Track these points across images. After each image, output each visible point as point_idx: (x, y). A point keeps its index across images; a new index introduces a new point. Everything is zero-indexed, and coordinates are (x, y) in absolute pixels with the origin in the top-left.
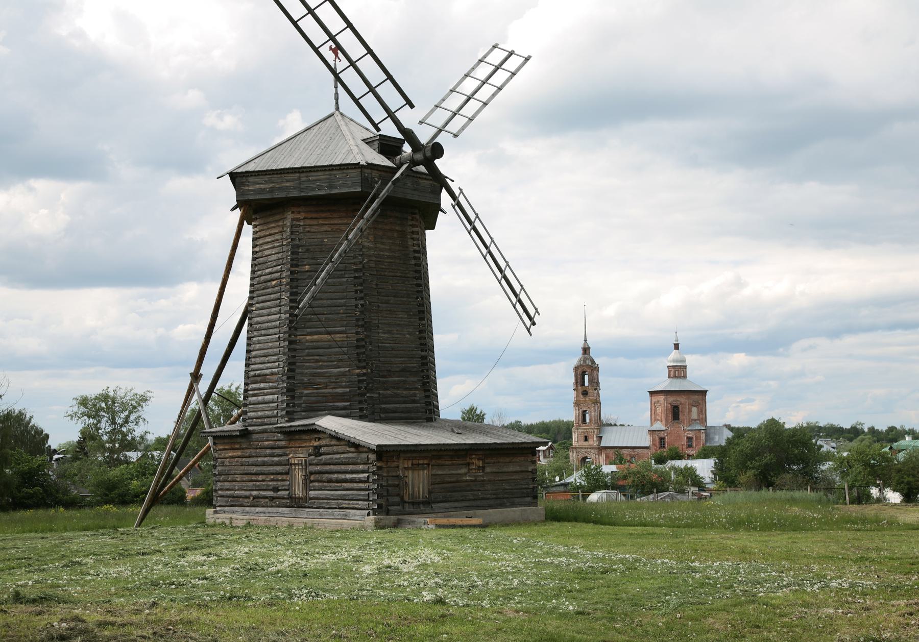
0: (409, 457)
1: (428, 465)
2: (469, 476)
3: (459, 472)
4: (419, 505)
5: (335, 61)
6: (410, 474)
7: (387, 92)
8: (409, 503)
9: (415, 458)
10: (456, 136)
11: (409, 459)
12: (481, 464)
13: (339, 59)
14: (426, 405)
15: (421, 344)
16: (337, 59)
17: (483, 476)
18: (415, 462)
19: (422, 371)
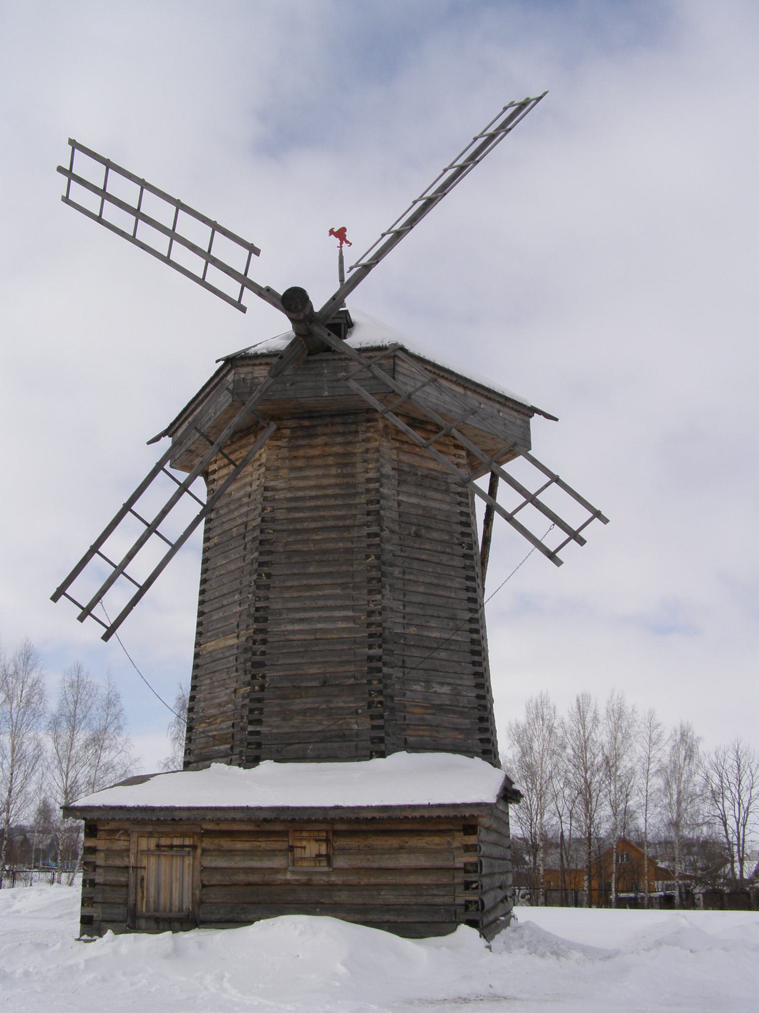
0: (151, 833)
1: (194, 847)
2: (293, 872)
3: (267, 863)
4: (170, 922)
5: (341, 247)
6: (151, 863)
7: (224, 250)
8: (148, 918)
9: (166, 835)
10: (66, 200)
11: (150, 835)
12: (323, 850)
13: (347, 242)
14: (373, 743)
15: (473, 642)
16: (344, 244)
17: (327, 874)
18: (164, 841)
19: (369, 682)
